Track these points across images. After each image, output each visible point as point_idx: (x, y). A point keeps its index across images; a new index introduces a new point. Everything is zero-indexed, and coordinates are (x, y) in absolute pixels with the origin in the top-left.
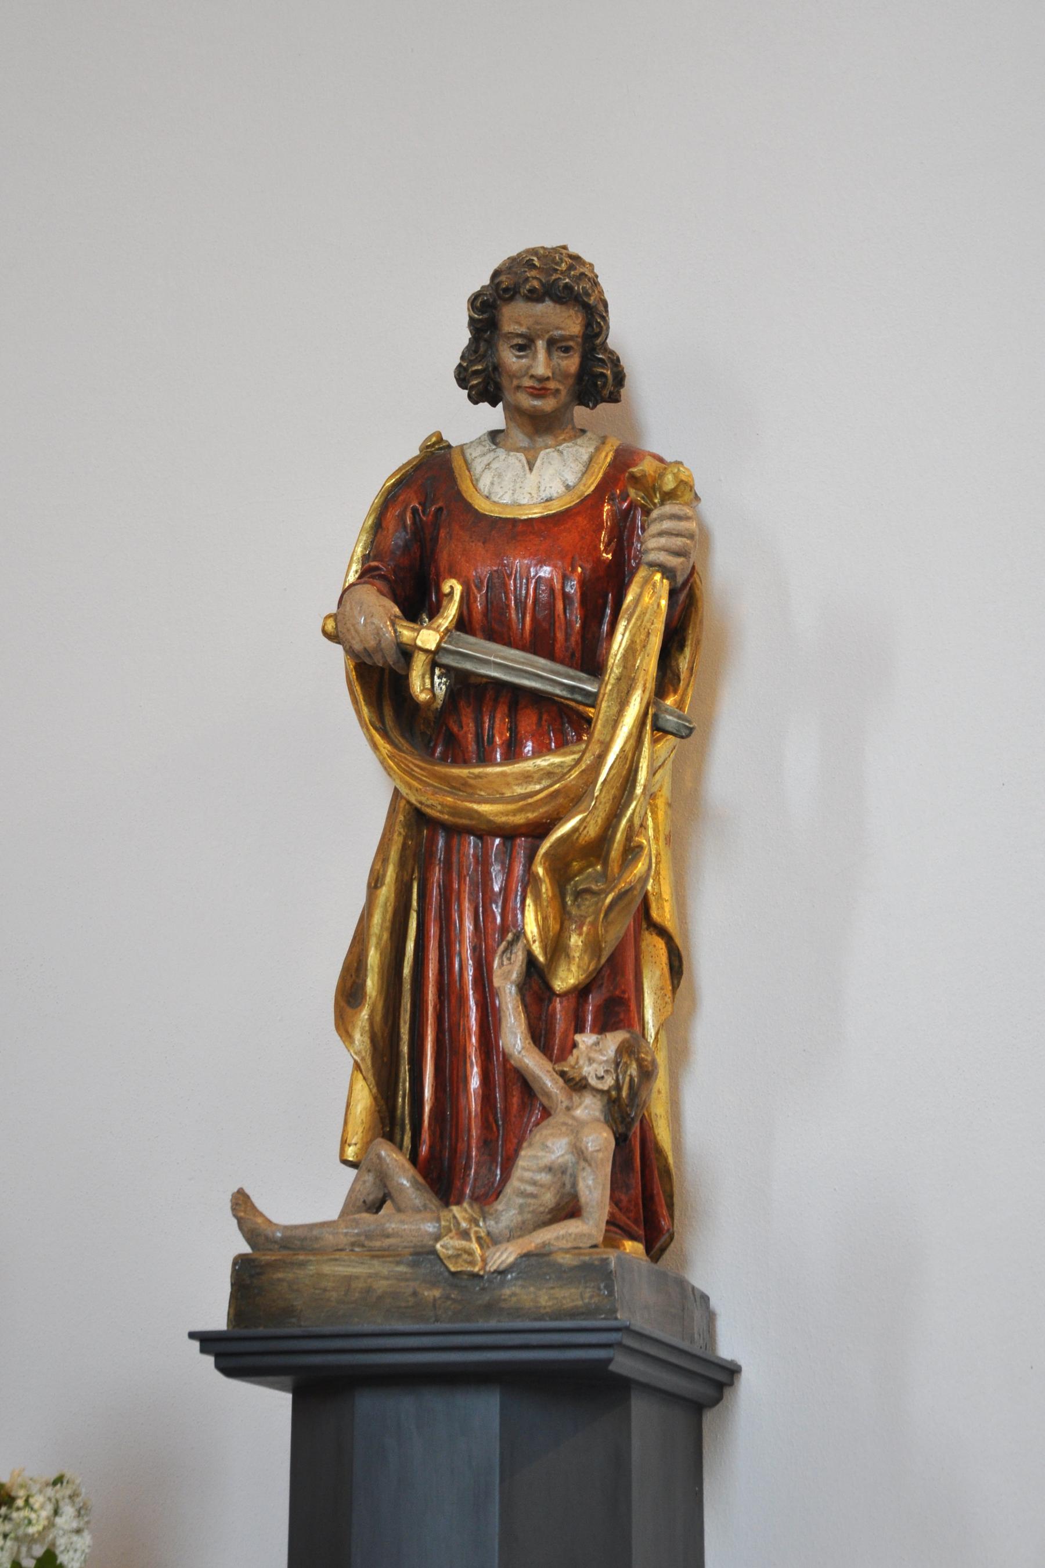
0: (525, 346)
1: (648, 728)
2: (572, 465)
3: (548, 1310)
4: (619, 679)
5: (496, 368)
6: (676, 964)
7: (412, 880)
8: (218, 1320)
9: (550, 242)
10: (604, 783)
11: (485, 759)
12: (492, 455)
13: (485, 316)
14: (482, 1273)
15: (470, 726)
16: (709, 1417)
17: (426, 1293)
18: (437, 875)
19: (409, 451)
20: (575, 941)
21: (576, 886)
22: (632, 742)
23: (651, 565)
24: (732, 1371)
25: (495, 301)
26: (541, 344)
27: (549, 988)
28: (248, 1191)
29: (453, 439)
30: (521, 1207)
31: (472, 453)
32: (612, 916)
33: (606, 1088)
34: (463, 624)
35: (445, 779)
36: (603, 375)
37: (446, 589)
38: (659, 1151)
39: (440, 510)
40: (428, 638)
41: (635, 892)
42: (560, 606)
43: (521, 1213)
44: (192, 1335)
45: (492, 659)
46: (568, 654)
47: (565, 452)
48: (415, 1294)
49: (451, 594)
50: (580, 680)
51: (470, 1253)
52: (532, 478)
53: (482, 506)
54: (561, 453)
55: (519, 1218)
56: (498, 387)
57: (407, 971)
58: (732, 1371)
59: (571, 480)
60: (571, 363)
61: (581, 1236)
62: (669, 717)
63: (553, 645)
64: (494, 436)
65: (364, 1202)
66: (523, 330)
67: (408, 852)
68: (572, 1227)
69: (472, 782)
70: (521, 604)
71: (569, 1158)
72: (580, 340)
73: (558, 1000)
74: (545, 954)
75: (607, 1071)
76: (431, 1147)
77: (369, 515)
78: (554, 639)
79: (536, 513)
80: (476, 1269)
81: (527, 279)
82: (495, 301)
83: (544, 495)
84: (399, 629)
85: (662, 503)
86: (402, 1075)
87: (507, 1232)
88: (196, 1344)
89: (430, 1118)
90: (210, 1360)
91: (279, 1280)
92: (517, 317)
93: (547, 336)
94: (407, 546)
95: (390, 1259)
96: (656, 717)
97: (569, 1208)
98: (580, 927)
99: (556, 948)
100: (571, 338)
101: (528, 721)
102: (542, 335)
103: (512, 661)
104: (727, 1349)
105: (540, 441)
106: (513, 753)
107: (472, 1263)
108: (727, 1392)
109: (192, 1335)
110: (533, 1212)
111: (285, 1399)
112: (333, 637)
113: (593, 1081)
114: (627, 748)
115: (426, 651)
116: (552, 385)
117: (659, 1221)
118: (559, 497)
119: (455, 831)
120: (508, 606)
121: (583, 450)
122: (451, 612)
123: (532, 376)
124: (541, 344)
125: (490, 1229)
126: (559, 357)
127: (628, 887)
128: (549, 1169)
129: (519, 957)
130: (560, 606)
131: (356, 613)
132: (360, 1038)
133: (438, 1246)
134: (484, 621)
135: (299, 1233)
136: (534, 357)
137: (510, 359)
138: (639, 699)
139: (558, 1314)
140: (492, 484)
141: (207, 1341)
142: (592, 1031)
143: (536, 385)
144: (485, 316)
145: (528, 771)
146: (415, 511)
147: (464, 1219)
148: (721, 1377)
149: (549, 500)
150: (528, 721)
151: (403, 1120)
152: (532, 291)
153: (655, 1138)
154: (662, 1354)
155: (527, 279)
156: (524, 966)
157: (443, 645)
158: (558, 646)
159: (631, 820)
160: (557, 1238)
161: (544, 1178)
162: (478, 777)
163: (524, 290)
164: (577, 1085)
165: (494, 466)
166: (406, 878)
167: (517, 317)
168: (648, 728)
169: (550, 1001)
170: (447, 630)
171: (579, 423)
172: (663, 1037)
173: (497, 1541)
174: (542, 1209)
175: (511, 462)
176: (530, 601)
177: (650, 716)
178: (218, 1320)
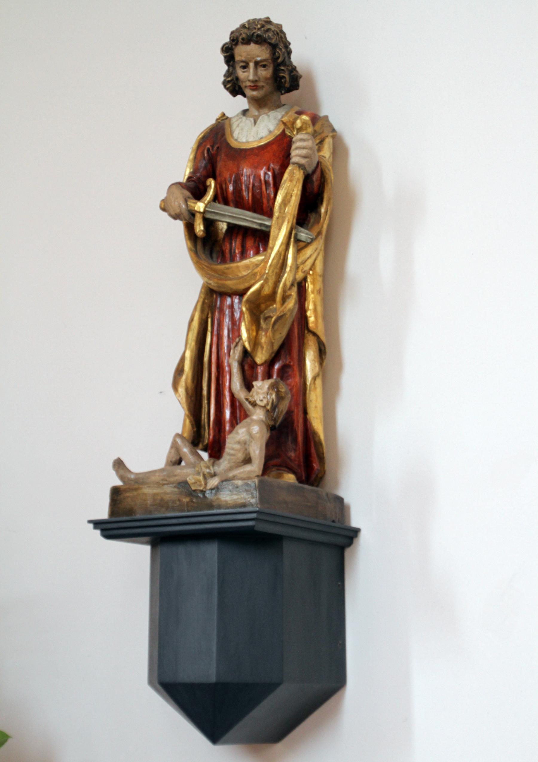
0: (245, 67)
1: (292, 240)
2: (273, 121)
3: (231, 505)
4: (278, 218)
5: (237, 79)
6: (323, 348)
7: (207, 318)
8: (104, 514)
9: (261, 15)
10: (271, 265)
11: (233, 260)
12: (240, 120)
13: (228, 54)
14: (204, 490)
15: (228, 246)
16: (348, 552)
17: (184, 500)
18: (217, 314)
19: (210, 121)
20: (263, 340)
21: (264, 315)
22: (284, 247)
23: (294, 163)
24: (356, 532)
25: (232, 46)
26: (252, 65)
27: (255, 363)
28: (123, 459)
29: (228, 114)
30: (229, 460)
31: (234, 120)
32: (276, 327)
33: (263, 405)
34: (215, 198)
35: (216, 271)
36: (284, 77)
37: (208, 184)
38: (315, 434)
39: (218, 148)
40: (200, 206)
41: (287, 316)
42: (264, 187)
43: (229, 463)
44: (90, 522)
45: (227, 214)
46: (269, 209)
47: (271, 116)
48: (179, 500)
49: (210, 185)
50: (263, 220)
51: (200, 481)
52: (255, 129)
53: (234, 144)
54: (269, 116)
55: (229, 465)
56: (240, 88)
57: (206, 359)
58: (356, 532)
59: (272, 128)
60: (265, 73)
61: (250, 472)
62: (302, 234)
63: (262, 206)
64: (245, 112)
65: (171, 461)
66: (243, 59)
67: (205, 305)
68: (248, 468)
69: (226, 271)
70: (248, 188)
71: (247, 437)
72: (270, 61)
73: (259, 367)
74: (250, 346)
75: (264, 397)
76: (214, 436)
77: (191, 153)
78: (262, 203)
79: (255, 145)
80: (201, 488)
81: (241, 34)
82: (232, 46)
83: (260, 136)
84: (189, 203)
85: (297, 133)
86: (203, 405)
87: (223, 471)
88: (91, 525)
89: (213, 424)
90: (98, 532)
91: (128, 497)
92: (242, 52)
93: (253, 61)
94: (205, 167)
95: (171, 485)
96: (296, 235)
97: (248, 460)
98: (266, 334)
99: (255, 342)
100: (265, 60)
101: (250, 243)
102: (262, 61)
103: (236, 214)
104: (355, 523)
105: (262, 111)
106: (244, 255)
107: (201, 485)
108: (355, 540)
109: (90, 522)
110: (234, 462)
111: (147, 549)
112: (164, 209)
113: (258, 402)
114: (281, 250)
115: (200, 212)
116: (260, 84)
117: (313, 465)
118: (266, 137)
119: (223, 294)
120: (242, 189)
121: (278, 114)
122: (211, 193)
123: (249, 81)
124: (252, 65)
125: (215, 471)
126: (261, 70)
127: (282, 314)
128: (239, 442)
129: (239, 348)
130: (264, 187)
131: (171, 197)
132: (182, 390)
133: (188, 479)
134: (221, 197)
135: (141, 476)
136: (249, 71)
137: (241, 73)
138: (285, 227)
139: (235, 506)
140: (239, 133)
141: (97, 524)
142: (263, 380)
143: (252, 84)
144: (228, 54)
145: (247, 264)
146: (208, 150)
147: (204, 467)
148: (351, 534)
149: (262, 138)
150: (250, 243)
151: (204, 425)
152: (243, 39)
153: (313, 428)
154: (292, 523)
155: (241, 34)
156: (241, 353)
157: (207, 209)
158: (264, 206)
159: (285, 285)
160: (240, 473)
161: (237, 447)
162: (228, 269)
163: (240, 40)
164: (254, 404)
165: (241, 125)
166: (204, 317)
167: (242, 52)
168: (292, 240)
169: (257, 368)
170: (209, 202)
171: (283, 102)
172: (319, 382)
173: (216, 607)
174: (238, 461)
175: (247, 122)
176: (251, 186)
177: (293, 235)
178: (104, 514)
